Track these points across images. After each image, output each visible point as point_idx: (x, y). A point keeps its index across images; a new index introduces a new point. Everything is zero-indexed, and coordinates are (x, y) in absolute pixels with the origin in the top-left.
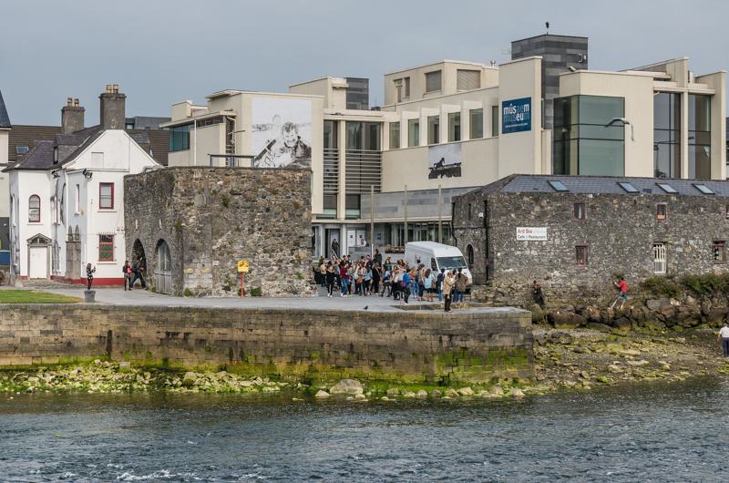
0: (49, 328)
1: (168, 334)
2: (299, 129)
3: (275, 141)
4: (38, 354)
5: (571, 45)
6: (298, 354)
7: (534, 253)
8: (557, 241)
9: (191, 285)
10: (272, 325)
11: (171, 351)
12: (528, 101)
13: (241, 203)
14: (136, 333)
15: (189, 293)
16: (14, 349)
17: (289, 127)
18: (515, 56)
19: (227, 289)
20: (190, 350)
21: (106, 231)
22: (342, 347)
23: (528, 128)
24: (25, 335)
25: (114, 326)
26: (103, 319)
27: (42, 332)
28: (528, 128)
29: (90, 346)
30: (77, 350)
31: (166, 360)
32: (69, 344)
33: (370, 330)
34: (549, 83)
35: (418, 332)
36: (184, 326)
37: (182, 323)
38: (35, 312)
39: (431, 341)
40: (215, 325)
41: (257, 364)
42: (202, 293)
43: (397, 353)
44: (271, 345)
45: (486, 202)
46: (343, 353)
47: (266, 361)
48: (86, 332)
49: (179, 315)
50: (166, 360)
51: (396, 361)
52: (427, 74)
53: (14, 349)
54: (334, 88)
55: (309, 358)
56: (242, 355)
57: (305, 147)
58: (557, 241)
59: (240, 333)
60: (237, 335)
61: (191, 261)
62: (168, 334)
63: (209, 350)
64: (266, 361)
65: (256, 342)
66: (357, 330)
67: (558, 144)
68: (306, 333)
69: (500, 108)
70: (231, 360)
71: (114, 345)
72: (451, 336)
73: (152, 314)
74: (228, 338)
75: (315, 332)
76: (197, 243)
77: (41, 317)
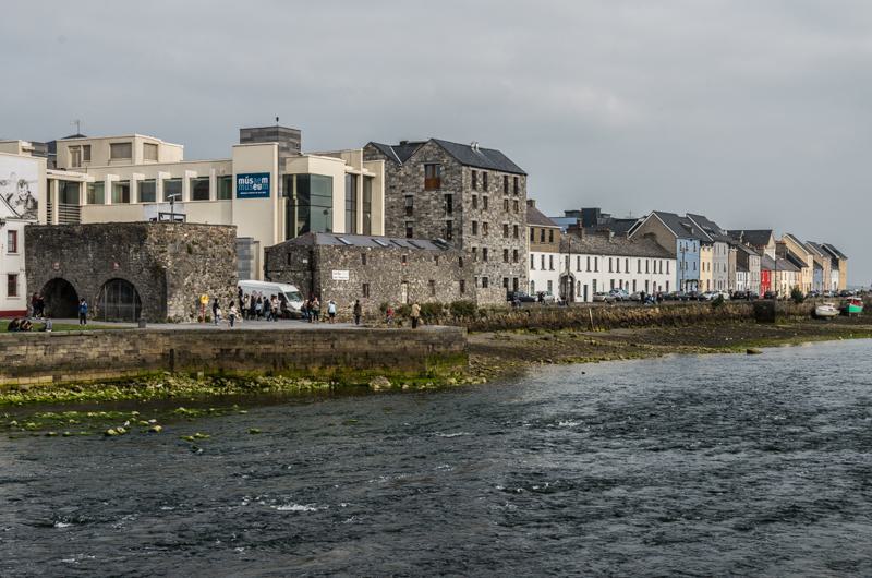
0: (130, 348)
1: (222, 350)
2: (30, 185)
3: (12, 195)
4: (124, 369)
5: (292, 135)
6: (327, 361)
7: (342, 289)
8: (354, 281)
9: (171, 314)
10: (306, 341)
11: (226, 362)
12: (268, 175)
13: (198, 251)
14: (194, 350)
15: (170, 321)
16: (108, 365)
17: (22, 183)
18: (243, 140)
19: (191, 316)
20: (242, 361)
21: (13, 271)
22: (359, 355)
23: (267, 195)
24: (115, 355)
25: (175, 346)
26: (167, 340)
27: (126, 352)
28: (267, 195)
29: (157, 362)
30: (149, 365)
31: (221, 370)
32: (144, 360)
33: (380, 342)
34: (282, 162)
35: (414, 343)
36: (235, 344)
37: (234, 342)
38: (121, 336)
39: (423, 348)
40: (261, 342)
41: (296, 370)
42: (178, 320)
43: (400, 358)
44: (306, 355)
45: (311, 252)
46: (360, 359)
47: (303, 367)
48: (154, 351)
49: (231, 336)
50: (221, 370)
51: (400, 363)
52: (112, 145)
53: (108, 365)
54: (24, 150)
55: (336, 364)
56: (284, 363)
57: (33, 200)
58: (354, 281)
59: (282, 347)
60: (279, 349)
61: (171, 296)
62: (222, 350)
63: (257, 361)
64: (303, 367)
65: (294, 354)
66: (370, 342)
67: (349, 213)
68: (332, 346)
69: (234, 179)
70: (275, 367)
71: (176, 360)
72: (433, 345)
73: (208, 336)
74: (272, 351)
75: (340, 345)
76: (174, 281)
77: (125, 340)
